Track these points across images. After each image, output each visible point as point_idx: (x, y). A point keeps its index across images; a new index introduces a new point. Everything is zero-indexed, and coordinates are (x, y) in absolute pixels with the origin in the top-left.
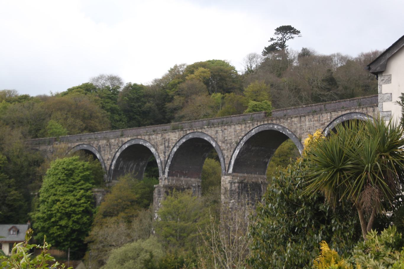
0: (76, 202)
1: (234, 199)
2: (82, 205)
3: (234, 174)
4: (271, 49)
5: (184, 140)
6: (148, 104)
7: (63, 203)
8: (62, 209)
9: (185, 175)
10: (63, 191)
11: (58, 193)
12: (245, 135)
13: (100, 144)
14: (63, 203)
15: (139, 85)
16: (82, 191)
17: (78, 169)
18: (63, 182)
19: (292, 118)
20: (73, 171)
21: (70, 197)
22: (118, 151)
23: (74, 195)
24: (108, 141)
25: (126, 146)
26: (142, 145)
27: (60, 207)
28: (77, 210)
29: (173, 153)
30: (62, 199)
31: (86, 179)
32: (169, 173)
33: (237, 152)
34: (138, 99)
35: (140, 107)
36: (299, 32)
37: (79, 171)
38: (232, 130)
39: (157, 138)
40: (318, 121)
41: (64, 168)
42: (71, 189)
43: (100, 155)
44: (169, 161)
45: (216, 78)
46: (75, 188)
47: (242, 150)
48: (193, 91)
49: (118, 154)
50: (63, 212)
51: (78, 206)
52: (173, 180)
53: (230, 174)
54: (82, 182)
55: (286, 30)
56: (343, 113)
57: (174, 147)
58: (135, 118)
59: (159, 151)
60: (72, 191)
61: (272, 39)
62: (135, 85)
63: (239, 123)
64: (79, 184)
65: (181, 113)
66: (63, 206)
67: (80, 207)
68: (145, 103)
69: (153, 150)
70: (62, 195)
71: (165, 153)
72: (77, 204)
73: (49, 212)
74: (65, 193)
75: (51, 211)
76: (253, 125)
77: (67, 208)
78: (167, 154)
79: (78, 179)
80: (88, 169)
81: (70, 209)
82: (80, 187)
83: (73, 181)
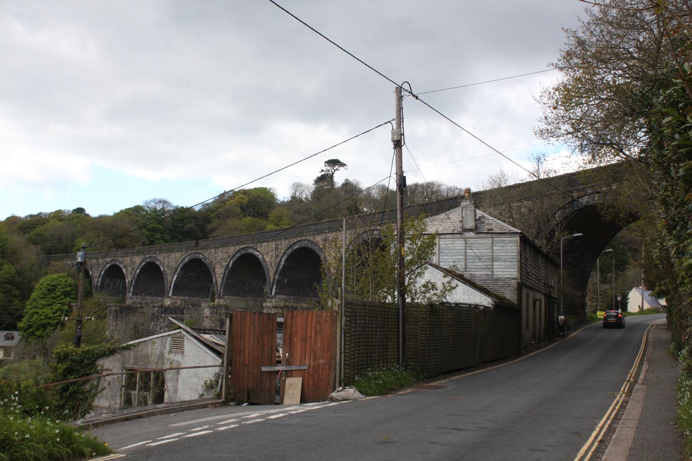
0: (51, 315)
1: (154, 322)
2: (56, 318)
3: (174, 297)
4: (320, 180)
5: (144, 264)
6: (189, 225)
7: (41, 315)
8: (38, 321)
9: (151, 295)
10: (43, 305)
11: (38, 306)
12: (181, 262)
13: (92, 262)
14: (41, 315)
15: (112, 216)
16: (59, 305)
17: (61, 285)
18: (44, 296)
19: (210, 249)
20: (56, 287)
21: (47, 311)
22: (102, 270)
23: (52, 309)
24: (97, 261)
25: (108, 265)
26: (118, 266)
27: (37, 319)
28: (51, 322)
29: (136, 275)
30: (40, 312)
31: (66, 294)
32: (133, 292)
33: (175, 277)
34: (182, 220)
35: (183, 227)
36: (345, 165)
37: (61, 287)
38: (174, 256)
39: (127, 260)
40: (227, 252)
41: (48, 284)
42: (50, 303)
43: (92, 272)
44: (133, 281)
45: (254, 205)
46: (54, 302)
47: (180, 275)
48: (229, 214)
49: (103, 273)
50: (39, 323)
51: (53, 319)
52: (137, 299)
53: (169, 297)
54: (62, 297)
55: (334, 163)
56: (243, 246)
57: (137, 270)
58: (177, 237)
59: (128, 272)
60: (51, 305)
61: (322, 171)
62: (182, 208)
63: (178, 251)
64: (59, 298)
65: (214, 234)
66: (40, 318)
67: (54, 319)
68: (187, 223)
69: (124, 270)
70: (41, 308)
71: (131, 274)
72: (53, 317)
73: (28, 323)
74: (45, 306)
75: (30, 322)
76: (187, 253)
77: (43, 320)
78: (133, 275)
79: (59, 294)
80: (70, 285)
81: (45, 321)
82: (58, 302)
83: (54, 295)
